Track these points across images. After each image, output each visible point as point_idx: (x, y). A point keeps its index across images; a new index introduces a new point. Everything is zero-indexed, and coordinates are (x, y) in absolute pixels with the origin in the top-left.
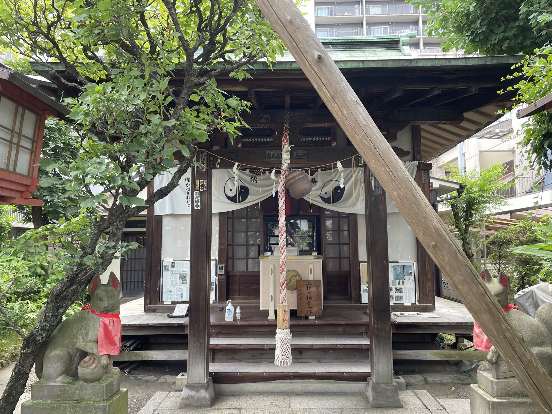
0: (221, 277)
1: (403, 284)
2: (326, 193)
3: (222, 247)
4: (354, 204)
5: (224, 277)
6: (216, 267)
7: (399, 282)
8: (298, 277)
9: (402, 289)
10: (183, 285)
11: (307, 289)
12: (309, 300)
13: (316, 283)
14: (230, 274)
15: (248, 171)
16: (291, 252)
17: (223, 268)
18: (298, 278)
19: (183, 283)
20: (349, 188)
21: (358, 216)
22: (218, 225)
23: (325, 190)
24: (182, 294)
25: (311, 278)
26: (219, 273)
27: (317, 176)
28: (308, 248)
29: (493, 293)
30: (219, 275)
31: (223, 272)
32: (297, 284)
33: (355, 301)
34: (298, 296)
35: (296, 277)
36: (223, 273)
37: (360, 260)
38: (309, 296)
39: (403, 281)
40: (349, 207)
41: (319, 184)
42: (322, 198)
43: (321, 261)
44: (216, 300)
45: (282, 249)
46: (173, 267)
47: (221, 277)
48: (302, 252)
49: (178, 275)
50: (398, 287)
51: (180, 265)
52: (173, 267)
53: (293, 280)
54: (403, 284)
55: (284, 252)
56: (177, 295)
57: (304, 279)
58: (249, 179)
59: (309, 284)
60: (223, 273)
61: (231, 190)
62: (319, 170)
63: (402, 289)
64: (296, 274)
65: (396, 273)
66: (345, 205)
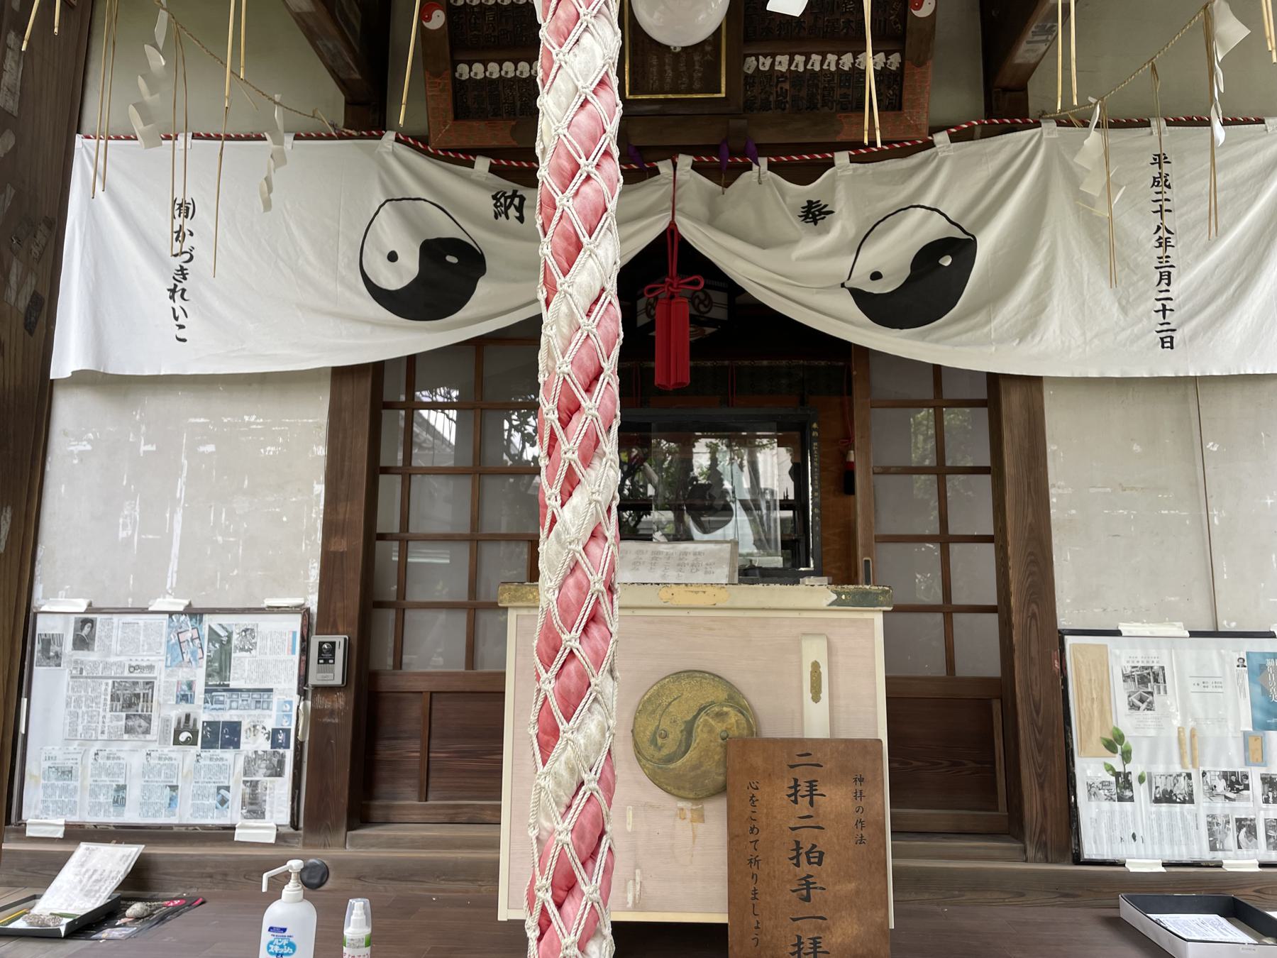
0: (325, 703)
2: (876, 276)
3: (341, 545)
4: (1030, 324)
5: (340, 702)
6: (305, 650)
8: (733, 717)
10: (130, 742)
11: (794, 796)
12: (805, 868)
13: (847, 755)
14: (385, 684)
15: (482, 164)
16: (695, 566)
17: (339, 653)
18: (872, 124)
19: (128, 730)
20: (995, 251)
21: (1048, 393)
22: (323, 433)
23: (873, 257)
24: (123, 788)
25: (816, 722)
26: (315, 679)
27: (832, 188)
28: (777, 561)
29: (463, 670)
30: (317, 689)
31: (335, 675)
32: (727, 759)
33: (1042, 845)
34: (733, 838)
35: (720, 716)
36: (338, 681)
37: (1063, 622)
38: (806, 838)
40: (1001, 341)
41: (842, 226)
42: (860, 297)
43: (878, 619)
44: (294, 824)
45: (570, 410)
46: (82, 642)
47: (325, 703)
48: (749, 574)
49: (106, 688)
51: (117, 634)
52: (82, 642)
53: (700, 735)
55: (590, 451)
56: (93, 793)
57: (770, 730)
58: (485, 203)
59: (804, 762)
60: (338, 681)
61: (393, 257)
62: (842, 158)
64: (723, 696)
66: (978, 333)
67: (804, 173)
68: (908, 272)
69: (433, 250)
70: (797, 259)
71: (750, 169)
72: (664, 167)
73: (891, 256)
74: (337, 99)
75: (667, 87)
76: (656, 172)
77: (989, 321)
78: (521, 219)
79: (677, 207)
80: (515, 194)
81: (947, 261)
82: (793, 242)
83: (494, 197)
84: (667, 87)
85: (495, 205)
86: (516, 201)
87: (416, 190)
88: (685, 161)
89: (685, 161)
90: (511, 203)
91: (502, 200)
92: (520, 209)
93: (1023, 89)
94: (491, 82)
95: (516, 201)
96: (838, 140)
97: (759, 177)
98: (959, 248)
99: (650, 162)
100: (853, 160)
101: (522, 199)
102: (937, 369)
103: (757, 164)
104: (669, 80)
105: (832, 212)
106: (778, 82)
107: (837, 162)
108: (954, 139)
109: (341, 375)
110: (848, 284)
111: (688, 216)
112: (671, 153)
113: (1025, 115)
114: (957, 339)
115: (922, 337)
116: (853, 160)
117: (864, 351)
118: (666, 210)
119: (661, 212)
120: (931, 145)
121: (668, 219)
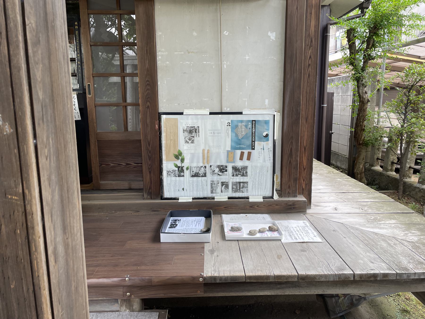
1: (249, 158)
7: (242, 154)
9: (245, 168)
39: (249, 154)
50: (239, 164)
54: (249, 158)
63: (245, 168)
65: (237, 135)
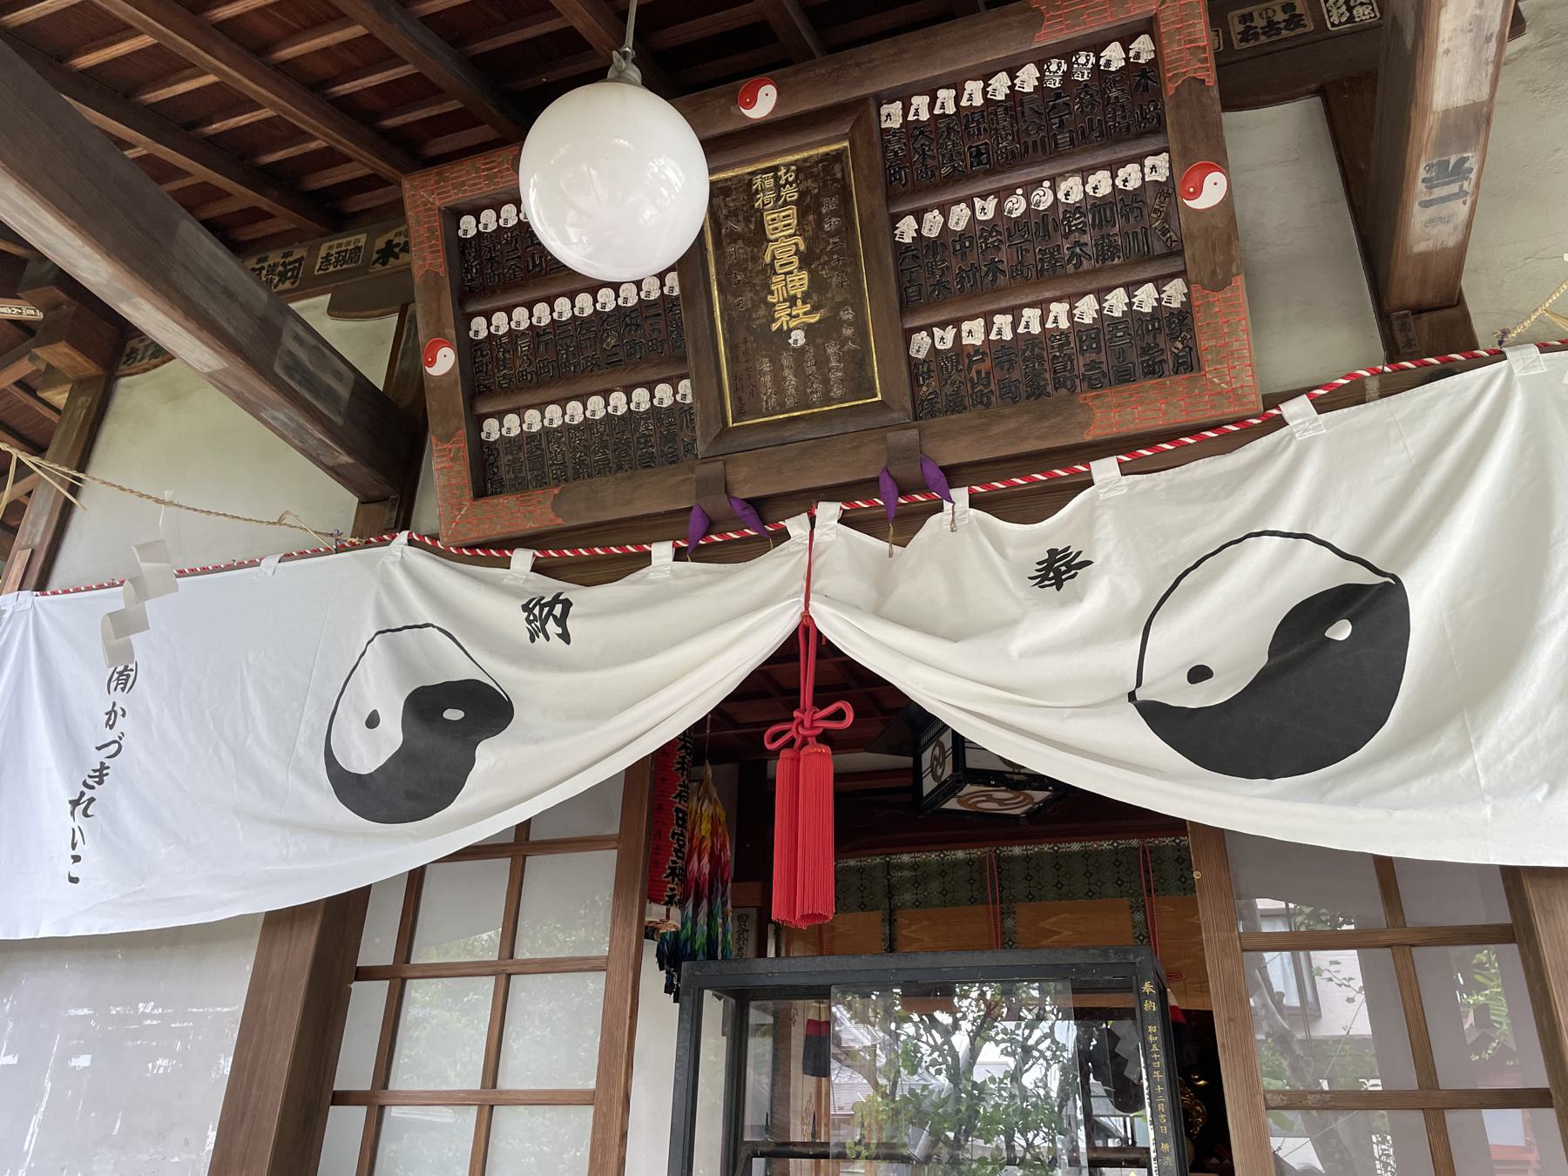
2: (1199, 674)
15: (522, 559)
42: (1159, 716)
58: (512, 618)
61: (373, 721)
67: (1026, 507)
68: (1263, 660)
69: (425, 705)
70: (1022, 655)
71: (940, 509)
72: (796, 526)
73: (1225, 632)
74: (348, 501)
75: (790, 402)
76: (784, 536)
77: (1466, 750)
78: (565, 637)
79: (815, 587)
80: (556, 600)
81: (1341, 631)
82: (1010, 624)
83: (525, 608)
84: (790, 402)
85: (527, 619)
86: (558, 610)
87: (424, 613)
88: (828, 512)
89: (828, 512)
90: (550, 613)
91: (536, 611)
92: (561, 621)
93: (1454, 301)
94: (531, 437)
95: (558, 610)
96: (1088, 437)
97: (958, 521)
98: (1374, 605)
99: (774, 523)
100: (1125, 470)
101: (567, 604)
102: (1384, 866)
103: (950, 500)
104: (792, 391)
105: (1088, 563)
106: (971, 363)
107: (1096, 478)
108: (1322, 406)
109: (278, 922)
110: (1141, 695)
111: (828, 599)
112: (805, 501)
113: (1469, 344)
114: (1398, 793)
115: (1320, 794)
116: (1125, 470)
117: (1217, 837)
118: (796, 594)
119: (790, 597)
120: (1280, 422)
121: (800, 608)
